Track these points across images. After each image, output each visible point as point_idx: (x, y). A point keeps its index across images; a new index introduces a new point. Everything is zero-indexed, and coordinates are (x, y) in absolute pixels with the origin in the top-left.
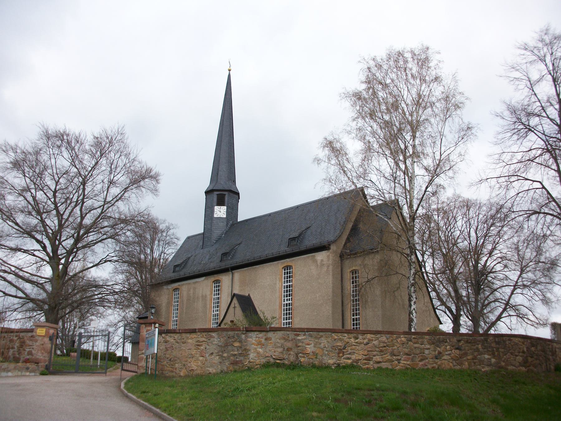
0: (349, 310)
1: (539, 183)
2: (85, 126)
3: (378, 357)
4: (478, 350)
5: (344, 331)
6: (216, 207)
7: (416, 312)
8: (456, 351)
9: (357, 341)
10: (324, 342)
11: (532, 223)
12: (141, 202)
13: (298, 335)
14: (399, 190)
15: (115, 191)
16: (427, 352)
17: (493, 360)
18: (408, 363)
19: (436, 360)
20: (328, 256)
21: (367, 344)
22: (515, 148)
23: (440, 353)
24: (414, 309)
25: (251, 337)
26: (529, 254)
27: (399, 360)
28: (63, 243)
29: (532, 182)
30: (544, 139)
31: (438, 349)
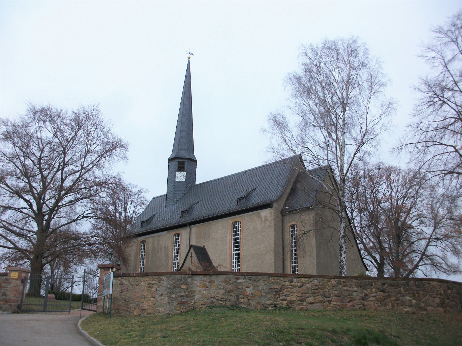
0: (289, 259)
1: (452, 147)
2: (68, 104)
3: (311, 298)
4: (400, 292)
5: (284, 275)
6: (177, 172)
7: (346, 260)
8: (380, 293)
9: (292, 284)
10: (263, 284)
11: (447, 182)
12: (113, 168)
13: (239, 279)
14: (331, 156)
15: (91, 158)
16: (354, 294)
17: (414, 302)
18: (338, 303)
19: (363, 302)
20: (271, 213)
21: (301, 286)
22: (431, 118)
23: (366, 295)
24: (344, 258)
25: (196, 280)
26: (442, 212)
27: (329, 302)
28: (47, 203)
29: (446, 147)
30: (456, 108)
31: (365, 291)
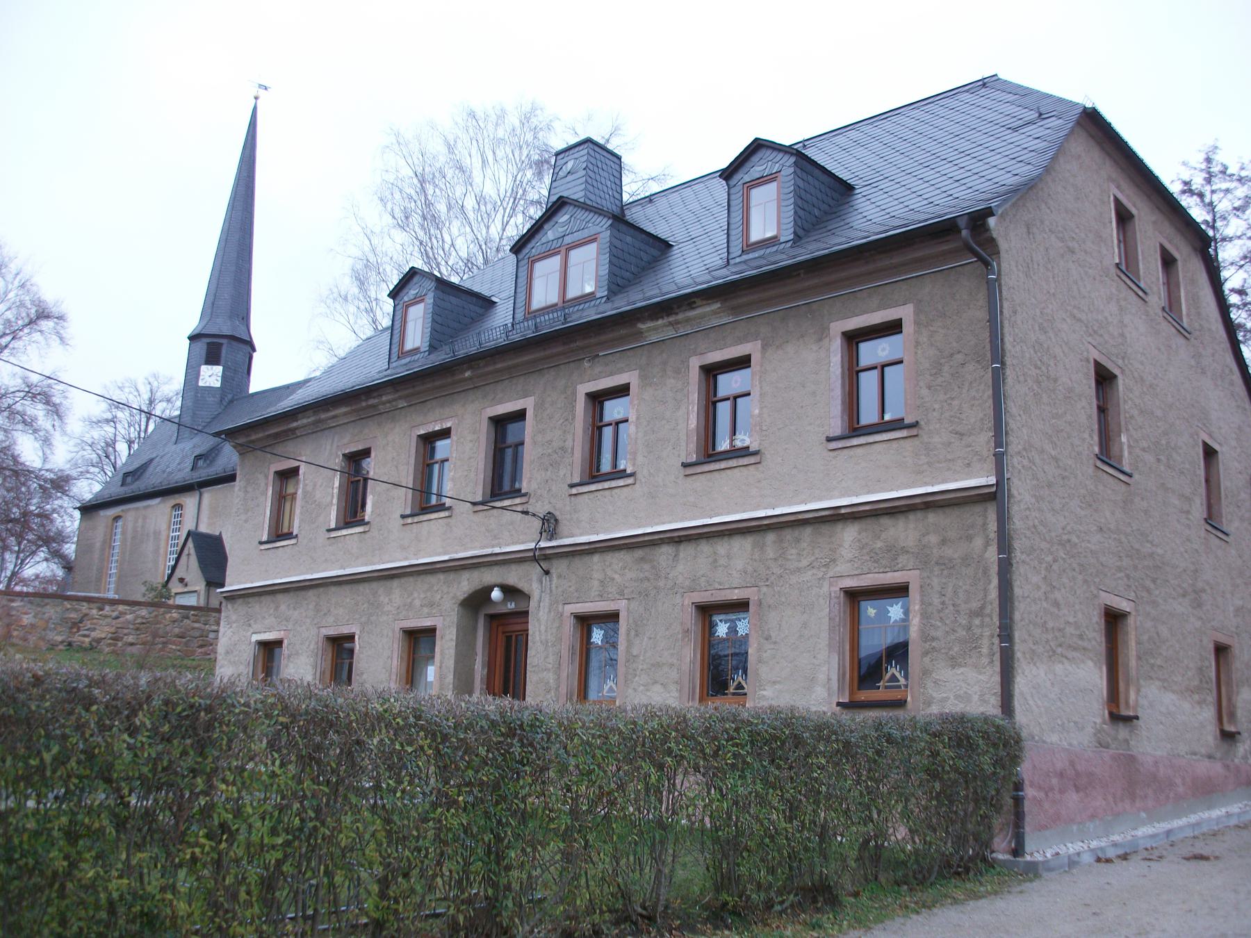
13: (13, 601)
